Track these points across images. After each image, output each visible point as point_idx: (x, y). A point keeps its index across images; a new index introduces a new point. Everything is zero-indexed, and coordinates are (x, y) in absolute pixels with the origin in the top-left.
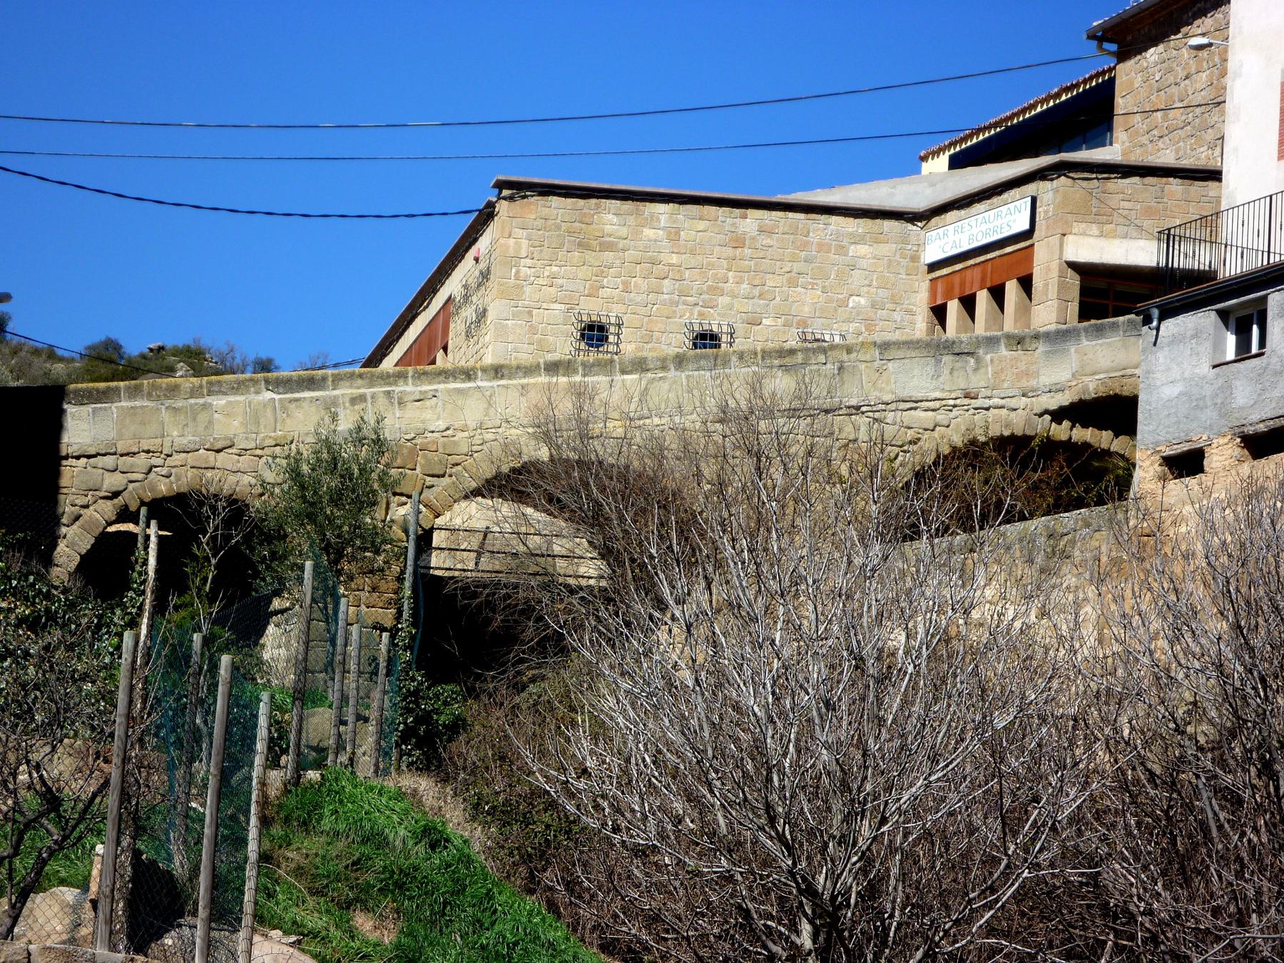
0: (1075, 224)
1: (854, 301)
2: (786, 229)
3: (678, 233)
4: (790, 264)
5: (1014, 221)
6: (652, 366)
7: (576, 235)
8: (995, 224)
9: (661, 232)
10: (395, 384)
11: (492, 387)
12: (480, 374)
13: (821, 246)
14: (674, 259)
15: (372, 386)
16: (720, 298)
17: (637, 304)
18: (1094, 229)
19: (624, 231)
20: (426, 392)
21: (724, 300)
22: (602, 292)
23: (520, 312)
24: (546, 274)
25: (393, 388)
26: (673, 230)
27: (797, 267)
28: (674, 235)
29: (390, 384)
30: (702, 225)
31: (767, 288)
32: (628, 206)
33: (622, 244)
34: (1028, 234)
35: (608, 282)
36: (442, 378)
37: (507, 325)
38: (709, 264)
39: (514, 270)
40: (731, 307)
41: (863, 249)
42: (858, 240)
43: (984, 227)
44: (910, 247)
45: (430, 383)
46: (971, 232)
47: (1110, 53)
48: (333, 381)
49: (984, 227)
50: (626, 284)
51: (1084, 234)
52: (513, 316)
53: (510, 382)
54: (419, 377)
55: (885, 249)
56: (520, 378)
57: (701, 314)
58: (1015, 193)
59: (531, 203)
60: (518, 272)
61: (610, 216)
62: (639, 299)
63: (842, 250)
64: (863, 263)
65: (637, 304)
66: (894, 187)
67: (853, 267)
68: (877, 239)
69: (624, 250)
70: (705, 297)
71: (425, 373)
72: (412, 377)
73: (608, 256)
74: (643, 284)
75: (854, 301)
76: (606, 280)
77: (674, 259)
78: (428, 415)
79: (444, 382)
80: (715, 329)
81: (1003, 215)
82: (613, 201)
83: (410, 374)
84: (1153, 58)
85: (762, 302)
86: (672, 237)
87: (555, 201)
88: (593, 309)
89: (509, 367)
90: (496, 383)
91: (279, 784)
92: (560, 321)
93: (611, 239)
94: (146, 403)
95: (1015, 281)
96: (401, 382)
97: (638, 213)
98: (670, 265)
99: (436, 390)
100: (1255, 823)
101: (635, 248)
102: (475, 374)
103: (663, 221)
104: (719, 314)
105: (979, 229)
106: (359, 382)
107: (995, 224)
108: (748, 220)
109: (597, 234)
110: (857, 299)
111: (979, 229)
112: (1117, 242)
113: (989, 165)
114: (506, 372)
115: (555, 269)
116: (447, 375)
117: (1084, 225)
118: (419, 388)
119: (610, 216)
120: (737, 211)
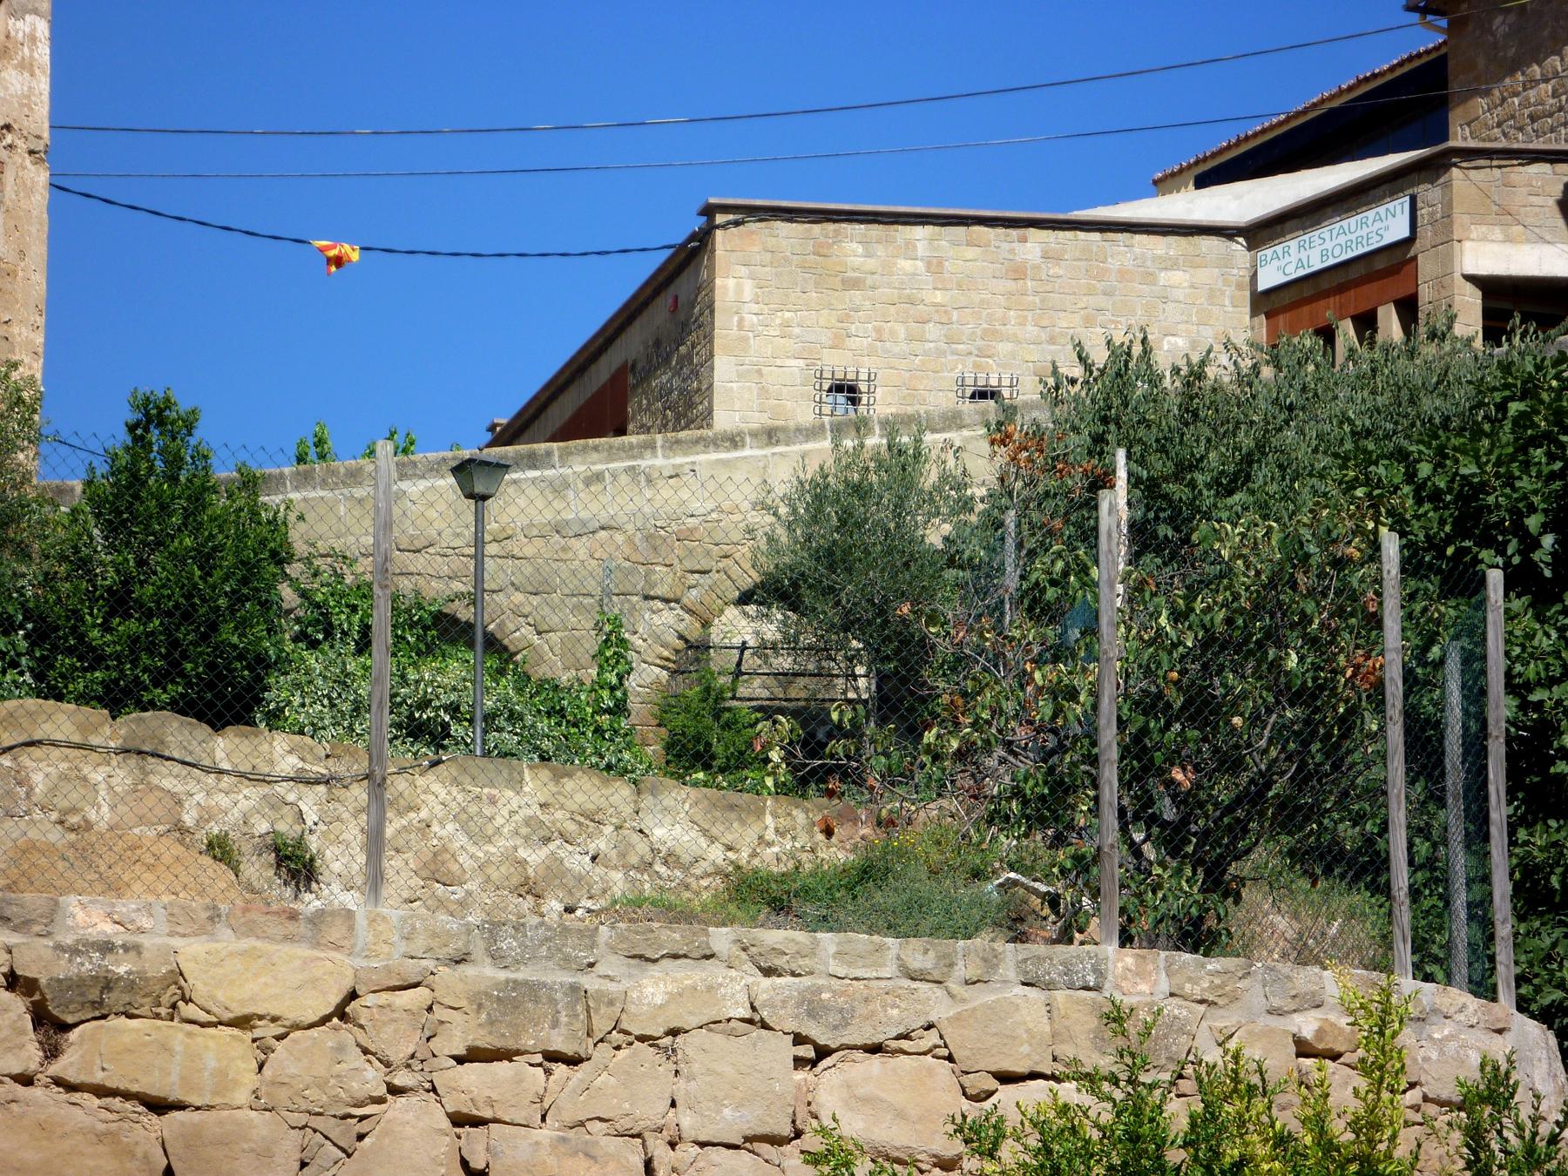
0: (1473, 227)
1: (1169, 343)
2: (1077, 254)
3: (940, 264)
4: (1085, 299)
5: (1387, 228)
6: (969, 422)
7: (813, 271)
8: (1359, 233)
9: (919, 264)
10: (641, 457)
11: (766, 456)
12: (748, 439)
13: (1123, 274)
14: (939, 297)
15: (610, 459)
16: (1001, 344)
17: (894, 356)
18: (1497, 233)
19: (871, 264)
20: (681, 466)
21: (1003, 348)
22: (851, 342)
23: (748, 371)
24: (778, 321)
25: (639, 462)
26: (935, 260)
27: (1094, 301)
28: (935, 266)
29: (634, 457)
30: (971, 253)
31: (1057, 330)
32: (875, 230)
33: (870, 280)
34: (1409, 241)
35: (857, 329)
36: (700, 447)
37: (732, 388)
38: (982, 301)
39: (736, 319)
40: (1013, 355)
41: (1178, 277)
42: (1171, 264)
43: (1342, 239)
44: (1235, 271)
45: (685, 454)
46: (1322, 247)
47: (1439, 29)
48: (560, 457)
49: (1342, 239)
50: (878, 331)
51: (1484, 239)
52: (738, 376)
53: (788, 449)
54: (671, 448)
55: (1206, 275)
56: (801, 443)
57: (975, 365)
58: (1393, 194)
59: (752, 233)
60: (741, 320)
61: (854, 245)
62: (896, 349)
63: (1149, 278)
64: (1179, 294)
65: (894, 356)
66: (1192, 201)
67: (1165, 300)
68: (1194, 263)
69: (873, 288)
70: (979, 343)
71: (678, 442)
72: (662, 447)
73: (856, 295)
74: (901, 331)
75: (1169, 343)
76: (854, 326)
77: (939, 297)
78: (685, 494)
79: (703, 452)
80: (994, 382)
81: (1370, 223)
82: (857, 226)
83: (659, 443)
84: (1502, 29)
85: (1053, 347)
86: (933, 268)
87: (782, 228)
88: (840, 364)
89: (784, 429)
90: (768, 451)
91: (1183, 1123)
92: (798, 381)
93: (857, 275)
94: (322, 493)
95: (1392, 305)
96: (648, 453)
97: (888, 241)
98: (935, 305)
99: (693, 463)
100: (1430, 955)
101: (889, 285)
102: (743, 440)
103: (921, 249)
104: (998, 365)
105: (1335, 242)
106: (595, 456)
107: (1359, 233)
108: (1028, 245)
109: (838, 268)
110: (1172, 339)
111: (1335, 242)
112: (1527, 248)
113: (1280, 177)
114: (782, 436)
115: (788, 315)
116: (716, 443)
117: (1484, 228)
118: (672, 461)
119: (853, 243)
120: (1014, 233)
